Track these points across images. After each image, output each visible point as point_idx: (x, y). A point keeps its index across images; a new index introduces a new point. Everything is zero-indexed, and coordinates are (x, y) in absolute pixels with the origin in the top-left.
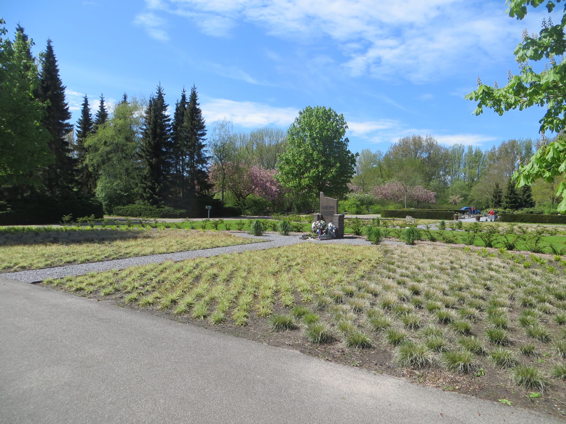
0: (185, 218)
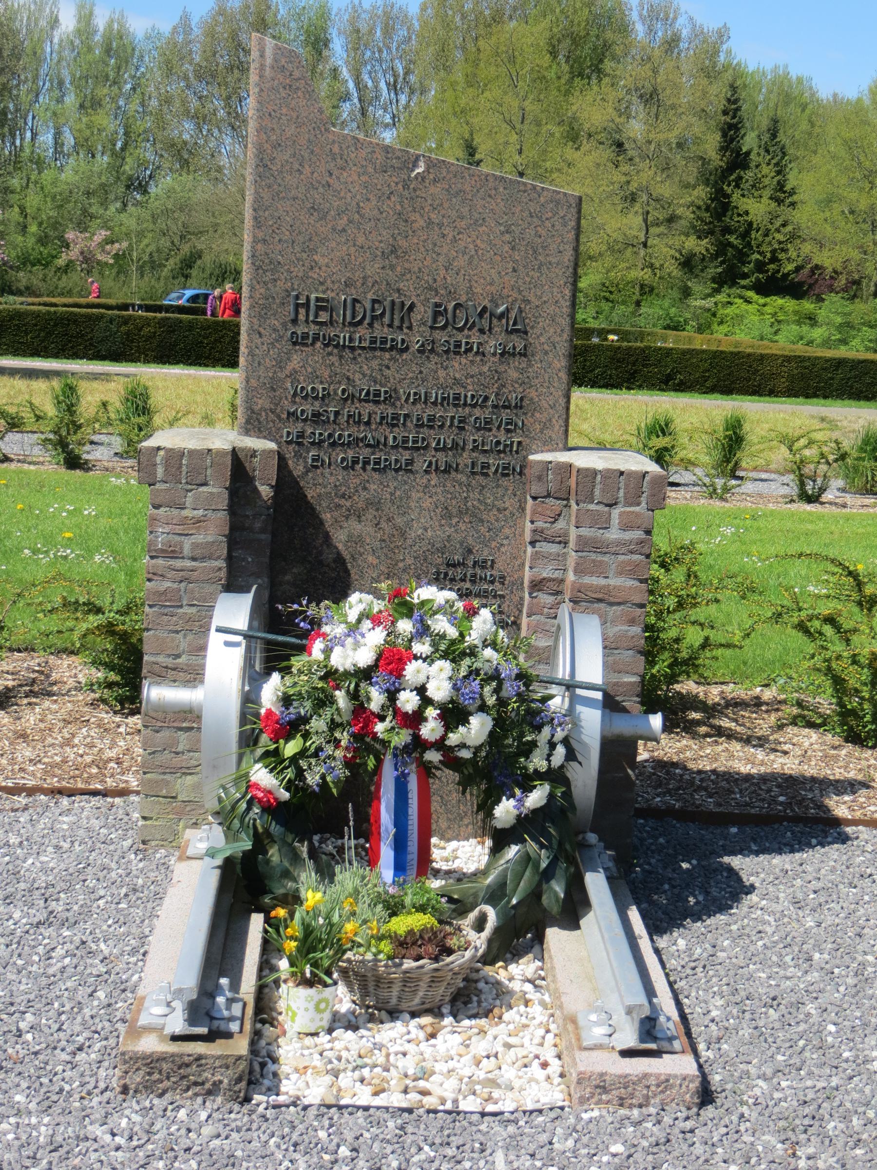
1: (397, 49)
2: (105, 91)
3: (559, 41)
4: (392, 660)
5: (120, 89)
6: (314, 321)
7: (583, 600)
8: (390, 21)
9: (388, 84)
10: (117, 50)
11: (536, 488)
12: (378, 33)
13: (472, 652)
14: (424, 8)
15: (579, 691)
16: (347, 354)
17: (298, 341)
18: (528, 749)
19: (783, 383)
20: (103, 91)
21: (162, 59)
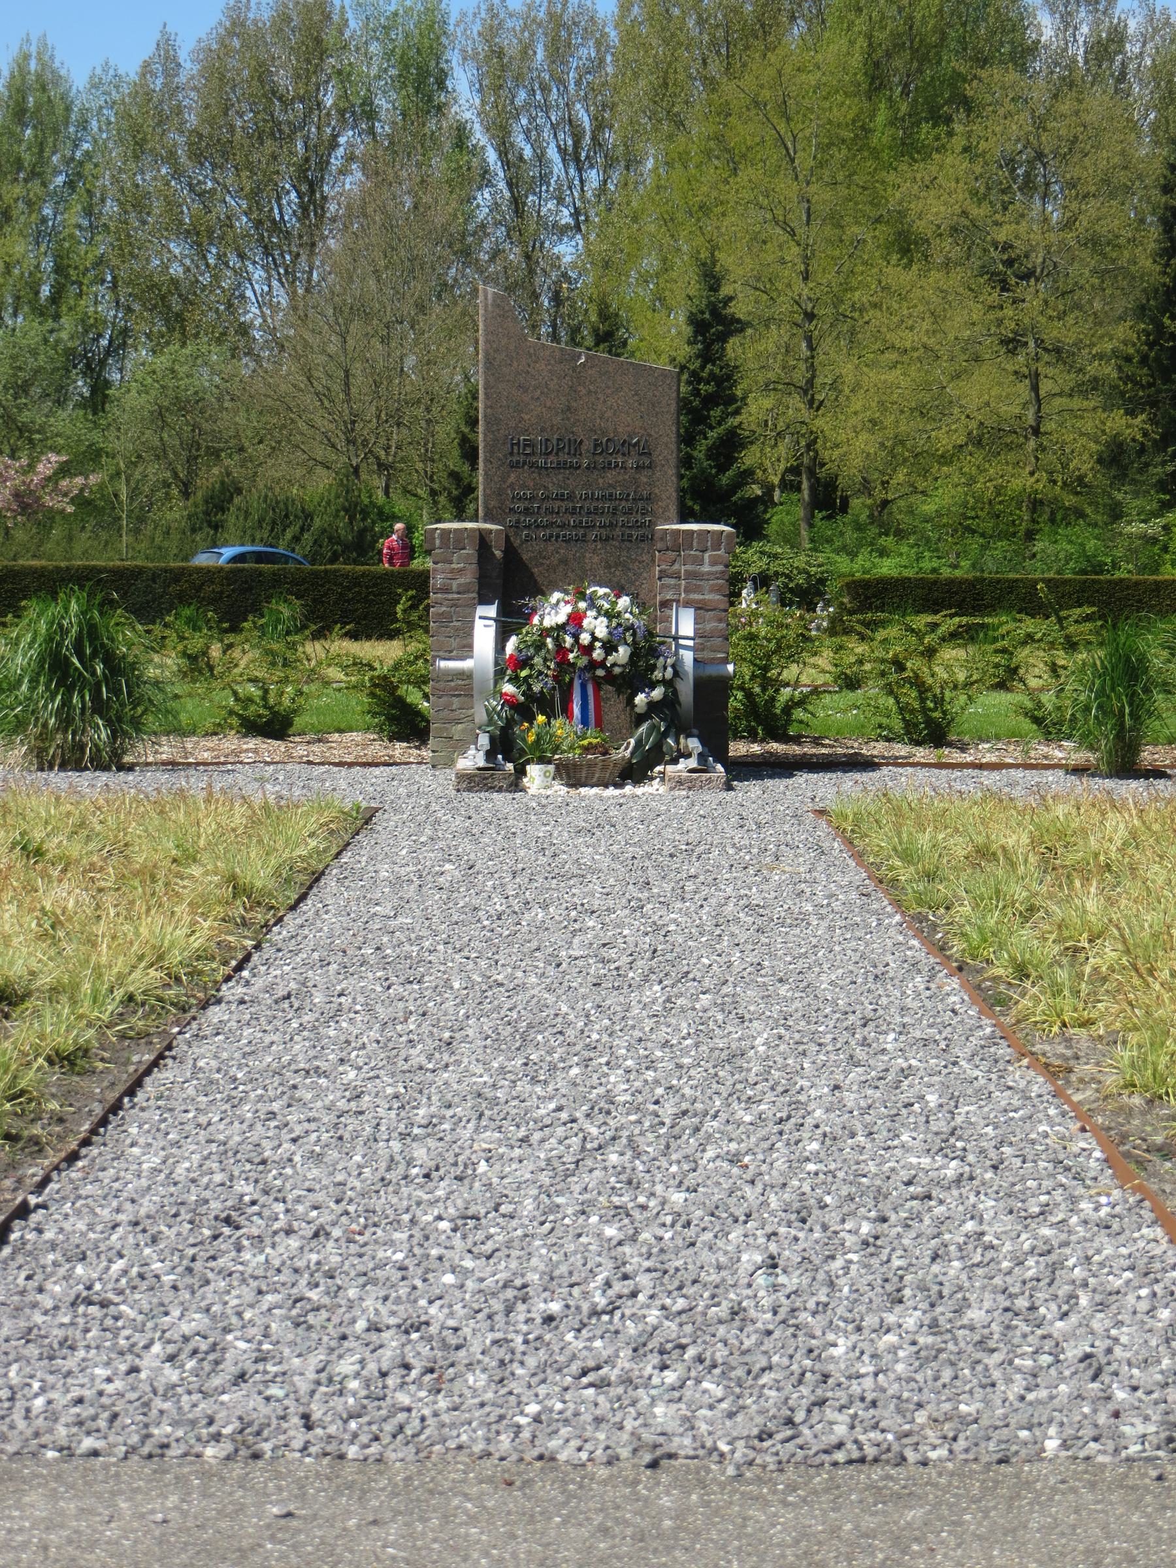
1: (578, 83)
2: (18, 190)
3: (888, 55)
4: (576, 619)
5: (44, 184)
6: (519, 454)
7: (687, 604)
8: (561, 33)
9: (562, 151)
11: (659, 545)
12: (540, 55)
13: (619, 615)
14: (625, 8)
15: (681, 642)
16: (544, 472)
17: (514, 466)
18: (653, 668)
21: (125, 125)
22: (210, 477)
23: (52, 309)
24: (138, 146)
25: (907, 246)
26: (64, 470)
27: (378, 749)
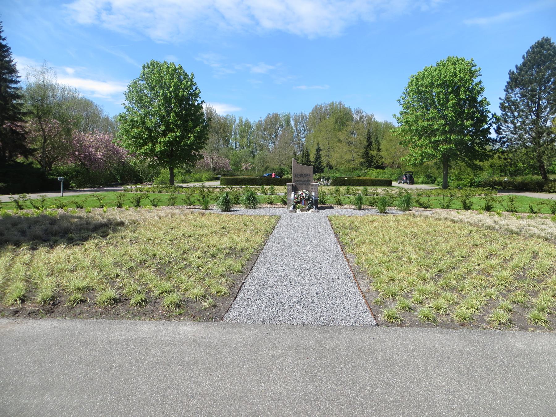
0: (9, 194)
4: (302, 194)
10: (247, 125)
19: (369, 184)
20: (245, 134)
22: (266, 165)
23: (249, 147)
24: (258, 130)
25: (340, 141)
26: (250, 165)
27: (282, 206)
